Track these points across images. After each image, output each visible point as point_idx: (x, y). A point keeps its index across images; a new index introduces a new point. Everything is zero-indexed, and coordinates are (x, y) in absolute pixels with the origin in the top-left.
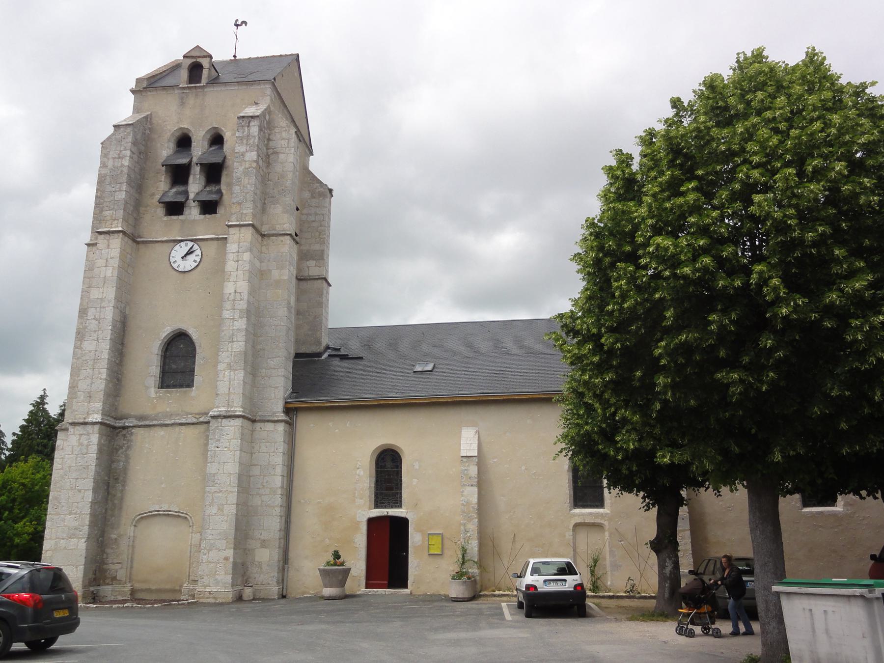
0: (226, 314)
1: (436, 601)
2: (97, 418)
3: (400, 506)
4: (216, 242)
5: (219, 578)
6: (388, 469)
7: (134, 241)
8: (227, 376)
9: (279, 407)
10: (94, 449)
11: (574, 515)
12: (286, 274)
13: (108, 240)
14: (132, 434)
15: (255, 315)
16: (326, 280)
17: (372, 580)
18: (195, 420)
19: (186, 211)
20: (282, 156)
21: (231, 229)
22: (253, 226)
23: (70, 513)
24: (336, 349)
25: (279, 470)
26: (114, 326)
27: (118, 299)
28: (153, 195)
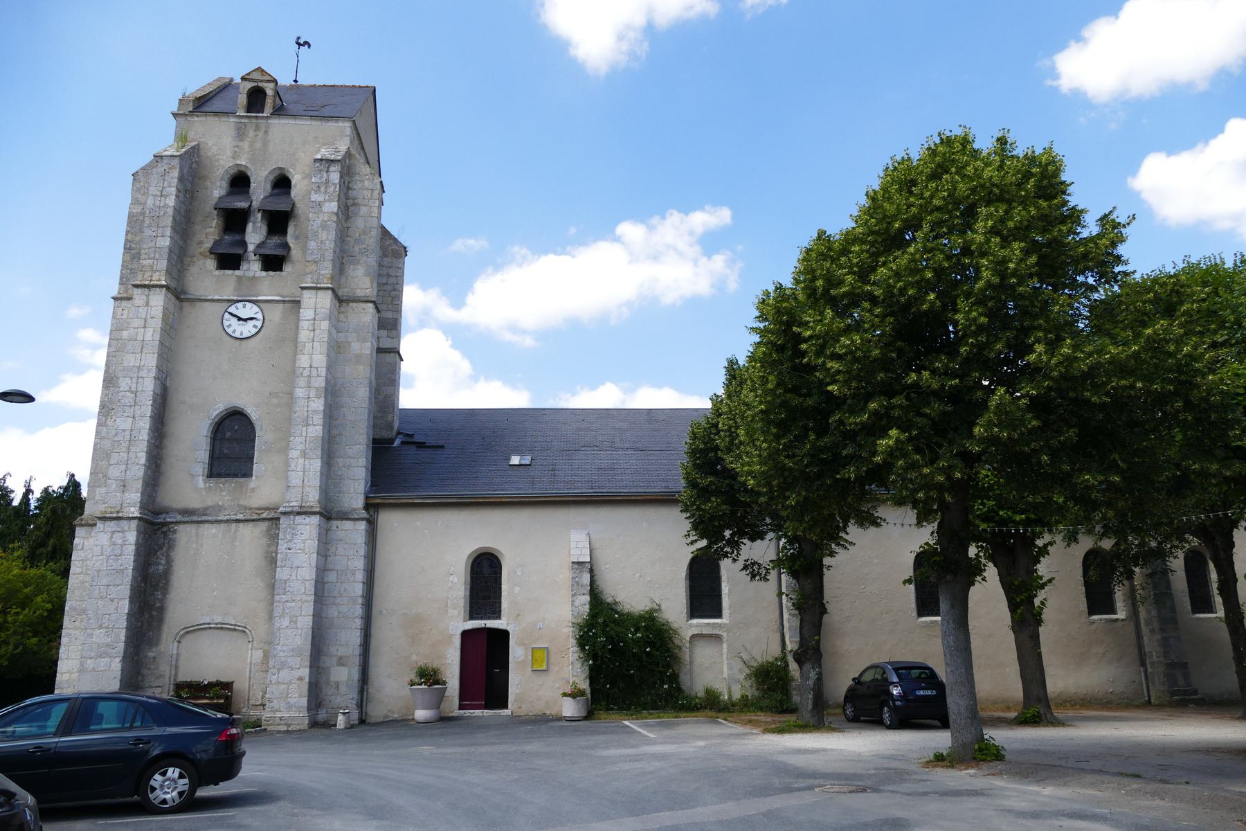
0: (300, 392)
1: (543, 722)
2: (137, 514)
3: (499, 617)
4: (281, 306)
5: (292, 701)
6: (485, 575)
7: (178, 298)
8: (300, 467)
9: (359, 502)
10: (131, 549)
11: (691, 626)
12: (365, 348)
13: (148, 296)
14: (175, 532)
15: (333, 393)
16: (398, 352)
17: (467, 699)
18: (255, 517)
19: (244, 266)
20: (363, 210)
21: (305, 292)
22: (374, 302)
23: (100, 627)
24: (408, 435)
25: (360, 576)
26: (154, 401)
27: (159, 369)
28: (201, 243)
